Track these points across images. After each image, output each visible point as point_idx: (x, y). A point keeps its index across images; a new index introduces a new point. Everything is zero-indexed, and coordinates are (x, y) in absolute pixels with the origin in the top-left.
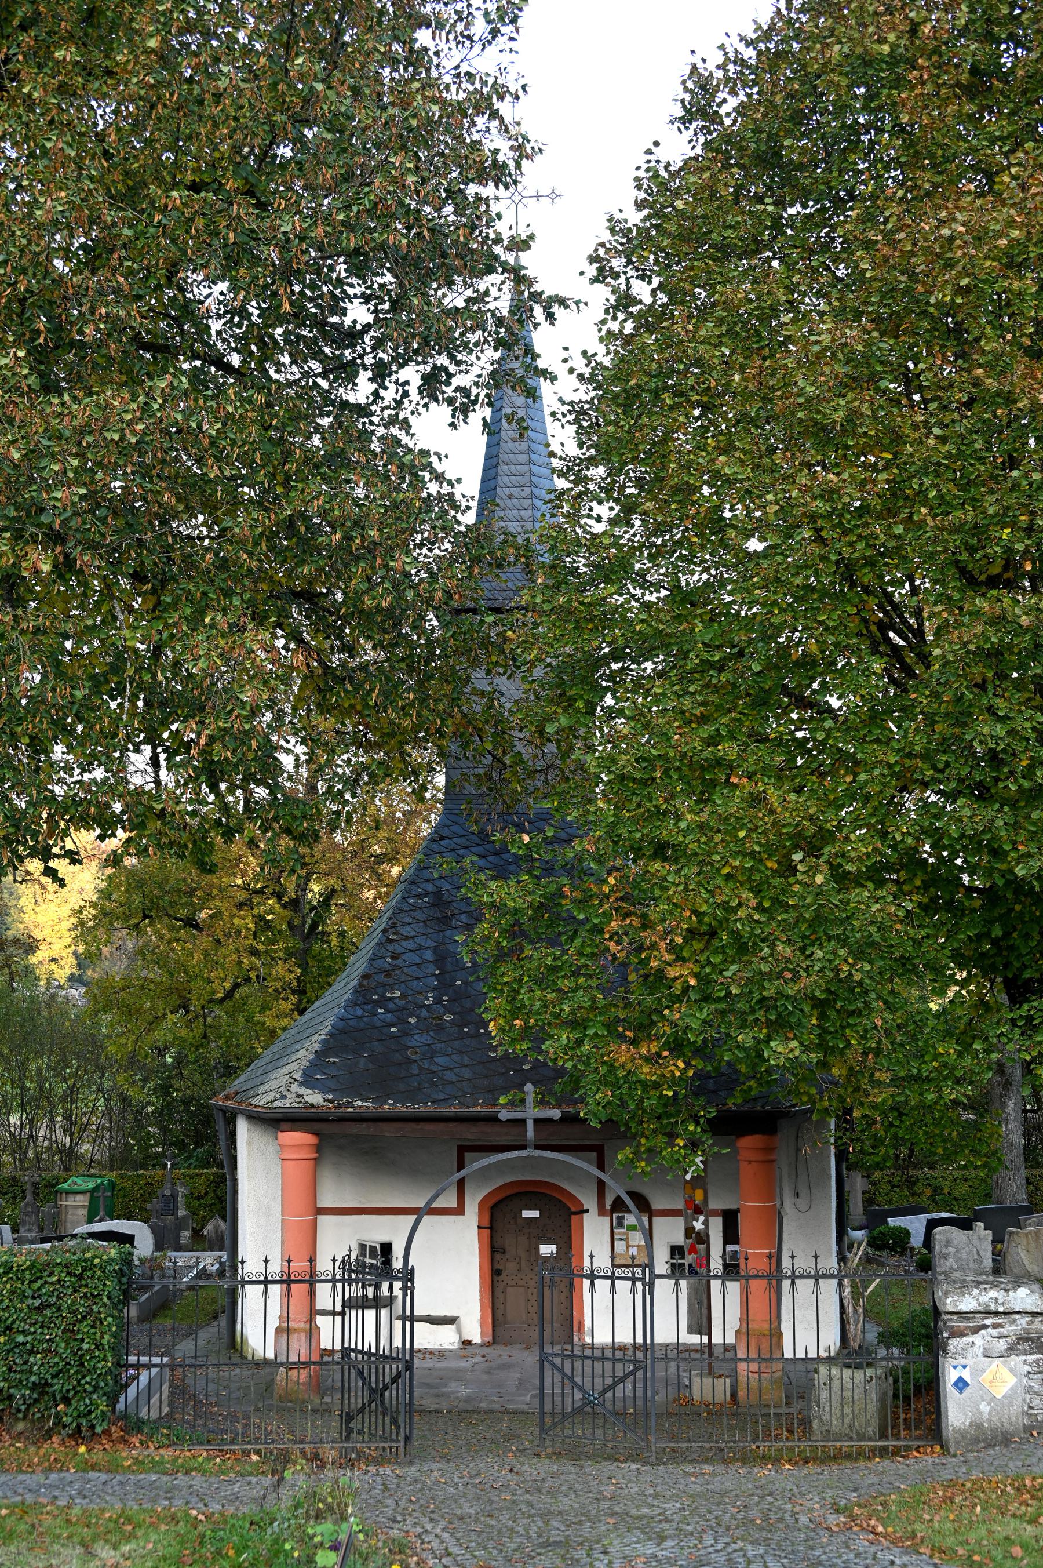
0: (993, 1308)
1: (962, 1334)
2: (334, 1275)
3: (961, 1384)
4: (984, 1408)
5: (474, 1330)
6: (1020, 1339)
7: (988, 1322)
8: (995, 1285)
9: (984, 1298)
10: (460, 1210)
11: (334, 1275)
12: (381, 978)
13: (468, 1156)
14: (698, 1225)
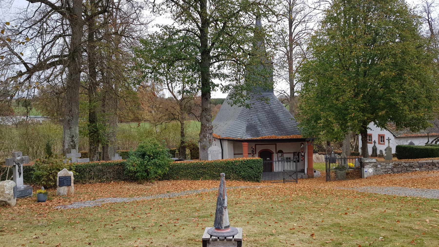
3: (366, 171)
4: (369, 174)
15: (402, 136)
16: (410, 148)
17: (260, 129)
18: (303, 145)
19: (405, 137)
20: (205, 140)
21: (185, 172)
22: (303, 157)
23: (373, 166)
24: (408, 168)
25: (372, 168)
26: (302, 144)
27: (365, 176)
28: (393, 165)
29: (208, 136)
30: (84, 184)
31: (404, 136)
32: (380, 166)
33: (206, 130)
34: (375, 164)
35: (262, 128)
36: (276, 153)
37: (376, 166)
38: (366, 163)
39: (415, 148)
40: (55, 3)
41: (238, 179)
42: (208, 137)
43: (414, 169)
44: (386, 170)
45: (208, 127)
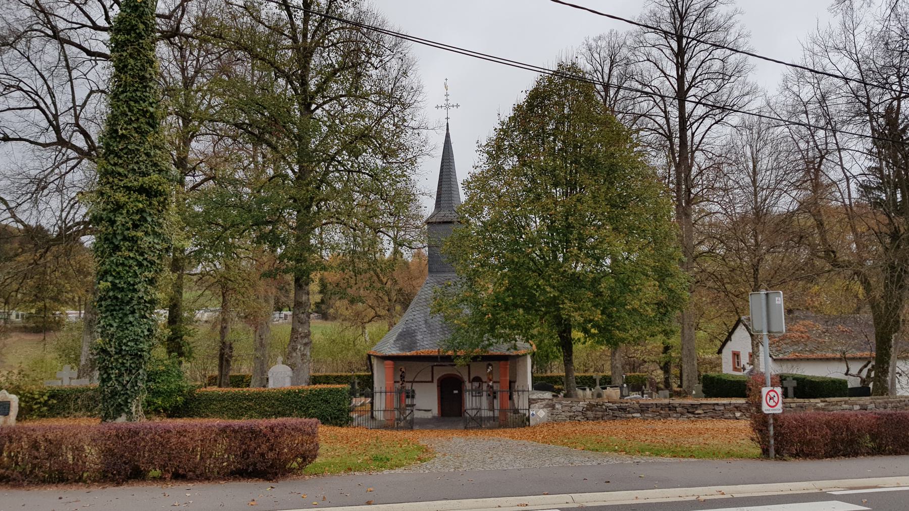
5: (435, 411)
10: (432, 382)
15: (786, 357)
16: (718, 379)
19: (794, 360)
21: (219, 406)
24: (617, 413)
25: (545, 409)
26: (490, 365)
27: (532, 422)
30: (66, 417)
31: (792, 356)
32: (560, 406)
33: (297, 338)
34: (550, 402)
36: (469, 382)
37: (553, 407)
38: (534, 400)
39: (725, 380)
42: (300, 350)
43: (630, 415)
44: (572, 414)
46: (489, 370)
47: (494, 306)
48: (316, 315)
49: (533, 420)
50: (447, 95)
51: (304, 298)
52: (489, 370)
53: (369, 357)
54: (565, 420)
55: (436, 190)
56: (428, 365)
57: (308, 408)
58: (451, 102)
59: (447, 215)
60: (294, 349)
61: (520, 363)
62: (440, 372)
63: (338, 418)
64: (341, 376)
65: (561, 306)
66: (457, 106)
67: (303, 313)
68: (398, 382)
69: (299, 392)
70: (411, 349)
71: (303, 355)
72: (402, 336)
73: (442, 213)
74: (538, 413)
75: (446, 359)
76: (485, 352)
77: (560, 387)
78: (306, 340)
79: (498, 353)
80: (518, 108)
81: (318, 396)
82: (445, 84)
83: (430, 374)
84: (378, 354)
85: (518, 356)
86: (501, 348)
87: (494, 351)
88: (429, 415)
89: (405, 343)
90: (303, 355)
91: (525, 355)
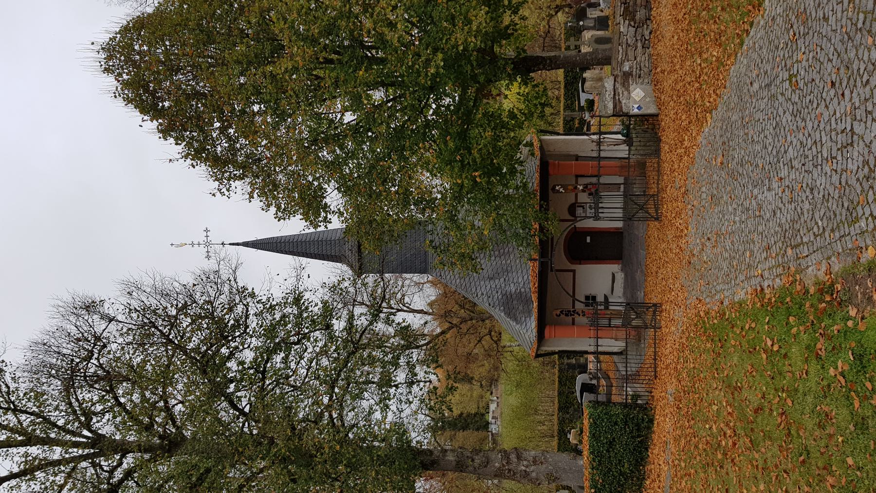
0: (612, 96)
1: (621, 107)
2: (601, 346)
3: (639, 108)
4: (648, 99)
5: (615, 268)
6: (624, 86)
7: (617, 98)
8: (605, 95)
9: (609, 99)
10: (574, 271)
11: (601, 346)
12: (490, 299)
13: (579, 179)
14: (581, 188)
17: (512, 285)
18: (557, 188)
20: (534, 475)
22: (589, 187)
23: (626, 86)
25: (631, 88)
26: (554, 188)
27: (652, 110)
28: (627, 22)
29: (524, 468)
33: (510, 470)
34: (619, 79)
35: (511, 279)
37: (627, 75)
38: (615, 107)
40: (292, 281)
41: (642, 479)
44: (639, 44)
45: (504, 465)
46: (561, 190)
47: (463, 167)
48: (493, 386)
49: (649, 108)
50: (193, 244)
51: (451, 457)
52: (561, 190)
53: (538, 356)
54: (650, 56)
55: (289, 257)
56: (551, 276)
57: (622, 474)
58: (202, 238)
59: (348, 249)
60: (526, 474)
61: (551, 148)
62: (560, 259)
63: (638, 425)
64: (559, 377)
65: (461, 48)
66: (207, 231)
67: (473, 460)
68: (573, 319)
69: (595, 487)
70: (528, 301)
71: (535, 462)
72: (510, 313)
73: (348, 253)
74: (638, 99)
75: (545, 248)
76: (535, 196)
77: (577, 122)
78: (513, 457)
79: (537, 175)
80: (165, 132)
81: (602, 456)
82: (178, 246)
83: (565, 273)
84: (536, 346)
85: (541, 148)
86: (531, 168)
87: (534, 183)
88: (620, 277)
89: (521, 308)
90: (535, 462)
91: (540, 141)
